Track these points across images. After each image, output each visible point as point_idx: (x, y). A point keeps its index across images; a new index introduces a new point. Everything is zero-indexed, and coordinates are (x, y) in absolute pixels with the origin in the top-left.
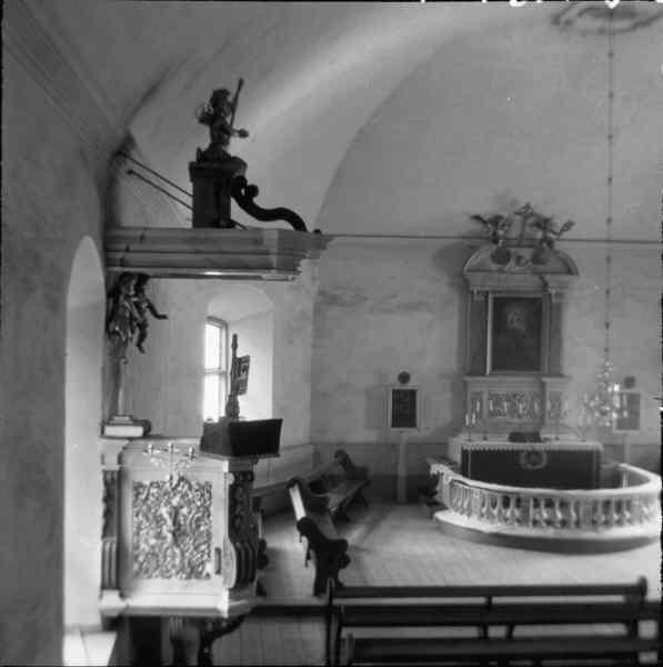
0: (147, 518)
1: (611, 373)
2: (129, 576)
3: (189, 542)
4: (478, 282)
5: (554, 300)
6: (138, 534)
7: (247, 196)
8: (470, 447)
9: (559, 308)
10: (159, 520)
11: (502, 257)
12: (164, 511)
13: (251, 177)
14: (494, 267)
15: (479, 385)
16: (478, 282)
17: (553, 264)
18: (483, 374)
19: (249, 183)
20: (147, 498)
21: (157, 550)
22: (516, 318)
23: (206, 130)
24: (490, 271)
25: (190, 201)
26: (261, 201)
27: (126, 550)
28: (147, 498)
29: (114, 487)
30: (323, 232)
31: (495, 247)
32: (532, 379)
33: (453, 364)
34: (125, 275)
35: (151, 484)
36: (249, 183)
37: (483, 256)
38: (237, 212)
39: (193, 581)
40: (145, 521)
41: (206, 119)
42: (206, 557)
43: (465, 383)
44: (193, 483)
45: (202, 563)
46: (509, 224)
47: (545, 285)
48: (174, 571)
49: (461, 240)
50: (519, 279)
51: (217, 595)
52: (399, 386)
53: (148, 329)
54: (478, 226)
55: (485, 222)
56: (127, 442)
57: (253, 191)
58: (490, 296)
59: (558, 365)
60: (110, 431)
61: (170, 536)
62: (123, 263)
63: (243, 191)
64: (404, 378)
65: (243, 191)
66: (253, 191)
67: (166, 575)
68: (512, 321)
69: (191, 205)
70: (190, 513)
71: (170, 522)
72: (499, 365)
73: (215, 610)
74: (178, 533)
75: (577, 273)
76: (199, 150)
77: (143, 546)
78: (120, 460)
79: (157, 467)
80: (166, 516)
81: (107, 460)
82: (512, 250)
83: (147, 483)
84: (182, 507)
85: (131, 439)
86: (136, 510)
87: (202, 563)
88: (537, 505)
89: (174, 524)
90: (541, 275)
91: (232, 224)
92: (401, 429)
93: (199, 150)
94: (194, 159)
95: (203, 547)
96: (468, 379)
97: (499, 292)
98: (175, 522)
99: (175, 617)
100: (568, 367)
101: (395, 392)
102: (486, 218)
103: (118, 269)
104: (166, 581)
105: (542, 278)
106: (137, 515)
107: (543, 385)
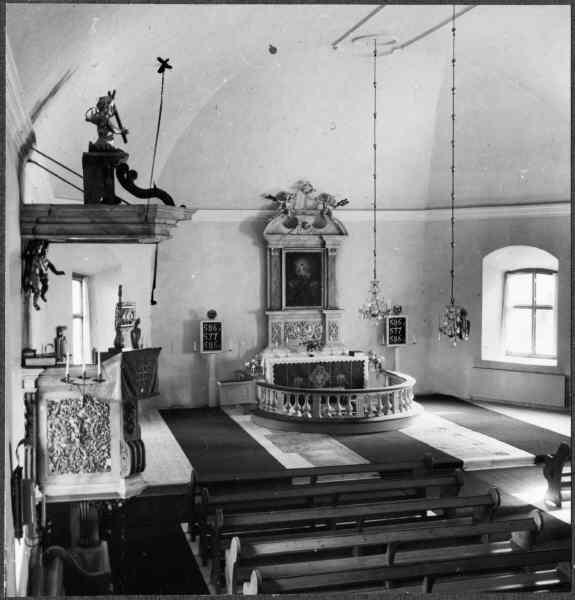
0: (59, 428)
2: (46, 475)
3: (92, 445)
4: (275, 242)
5: (330, 254)
6: (52, 440)
7: (128, 178)
8: (279, 361)
9: (334, 259)
10: (70, 429)
11: (292, 224)
12: (72, 421)
13: (132, 164)
14: (286, 230)
15: (278, 318)
16: (275, 242)
17: (330, 228)
18: (280, 309)
19: (130, 169)
20: (59, 413)
21: (67, 452)
22: (302, 267)
23: (94, 128)
24: (283, 234)
25: (80, 183)
26: (142, 183)
27: (43, 451)
28: (59, 413)
29: (32, 403)
30: (188, 206)
31: (285, 217)
32: (316, 312)
33: (256, 304)
34: (37, 240)
35: (62, 402)
36: (130, 169)
37: (277, 223)
38: (120, 191)
39: (97, 473)
40: (57, 430)
41: (93, 120)
42: (106, 455)
43: (267, 317)
44: (94, 399)
45: (104, 459)
46: (293, 197)
47: (323, 244)
48: (81, 467)
49: (422, 216)
51: (115, 482)
53: (49, 283)
54: (270, 202)
55: (274, 199)
56: (41, 371)
57: (134, 174)
58: (284, 252)
60: (29, 362)
61: (78, 440)
62: (34, 232)
63: (125, 175)
65: (125, 175)
66: (134, 174)
67: (75, 471)
69: (82, 187)
70: (92, 421)
71: (77, 431)
73: (116, 494)
74: (84, 437)
75: (346, 234)
76: (91, 143)
77: (56, 448)
78: (36, 386)
79: (57, 393)
80: (74, 425)
81: (26, 385)
82: (298, 217)
83: (57, 400)
84: (86, 418)
85: (45, 367)
86: (50, 422)
87: (104, 459)
88: (324, 401)
89: (81, 431)
90: (321, 236)
91: (118, 201)
93: (91, 143)
94: (86, 150)
95: (104, 447)
96: (267, 313)
98: (82, 430)
99: (83, 502)
100: (341, 302)
102: (274, 195)
103: (30, 237)
104: (76, 475)
105: (321, 238)
106: (51, 427)
107: (324, 316)
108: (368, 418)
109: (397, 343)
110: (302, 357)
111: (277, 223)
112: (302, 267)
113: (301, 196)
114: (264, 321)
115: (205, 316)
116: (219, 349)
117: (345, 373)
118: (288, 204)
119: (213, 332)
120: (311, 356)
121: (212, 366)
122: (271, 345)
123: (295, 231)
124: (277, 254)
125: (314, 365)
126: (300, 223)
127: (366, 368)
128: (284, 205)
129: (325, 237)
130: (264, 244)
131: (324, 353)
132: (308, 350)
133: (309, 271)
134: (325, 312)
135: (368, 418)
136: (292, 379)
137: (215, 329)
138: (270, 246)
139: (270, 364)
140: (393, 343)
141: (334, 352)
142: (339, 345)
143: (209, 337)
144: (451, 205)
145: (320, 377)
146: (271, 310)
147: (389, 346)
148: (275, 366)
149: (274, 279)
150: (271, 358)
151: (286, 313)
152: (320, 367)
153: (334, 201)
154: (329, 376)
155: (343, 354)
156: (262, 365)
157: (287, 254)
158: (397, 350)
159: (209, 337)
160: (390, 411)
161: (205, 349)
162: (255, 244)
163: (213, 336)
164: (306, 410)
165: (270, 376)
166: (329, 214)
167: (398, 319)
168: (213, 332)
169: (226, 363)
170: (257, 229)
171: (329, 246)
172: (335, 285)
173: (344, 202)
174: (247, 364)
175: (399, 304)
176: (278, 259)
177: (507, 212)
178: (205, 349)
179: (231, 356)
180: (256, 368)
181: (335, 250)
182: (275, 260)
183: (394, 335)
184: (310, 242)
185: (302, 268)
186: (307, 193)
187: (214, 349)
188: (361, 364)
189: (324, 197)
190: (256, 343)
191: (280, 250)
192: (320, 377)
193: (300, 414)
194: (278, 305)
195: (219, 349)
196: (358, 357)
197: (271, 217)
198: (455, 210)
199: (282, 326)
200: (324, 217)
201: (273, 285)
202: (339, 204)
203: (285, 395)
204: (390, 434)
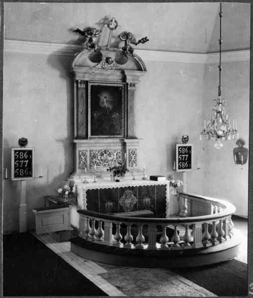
11: (97, 58)
15: (83, 146)
18: (86, 137)
22: (105, 100)
31: (93, 50)
32: (117, 140)
33: (64, 133)
37: (84, 57)
47: (124, 79)
58: (90, 85)
75: (145, 70)
90: (123, 72)
96: (75, 141)
107: (124, 144)
108: (206, 248)
109: (185, 168)
110: (107, 182)
111: (84, 57)
112: (105, 100)
113: (106, 31)
114: (72, 148)
115: (17, 143)
116: (30, 176)
117: (150, 197)
118: (94, 39)
119: (24, 159)
120: (118, 181)
121: (23, 193)
122: (78, 171)
123: (99, 66)
124: (83, 86)
125: (123, 190)
126: (104, 58)
127: (168, 191)
128: (91, 40)
129: (126, 73)
130: (70, 75)
131: (125, 178)
132: (115, 176)
133: (111, 103)
134: (126, 141)
135: (206, 248)
136: (103, 202)
137: (26, 156)
138: (77, 78)
139: (84, 190)
140: (182, 168)
141: (136, 178)
142: (138, 171)
143: (20, 164)
144: (222, 53)
145: (129, 201)
146: (78, 138)
147: (178, 171)
148: (211, 214)
149: (80, 110)
150: (84, 183)
151: (92, 141)
152: (128, 191)
153: (135, 39)
154: (136, 200)
155: (144, 179)
156: (74, 191)
157: (92, 86)
158: (185, 174)
159: (20, 164)
160: (217, 242)
161: (16, 176)
162: (61, 76)
163: (24, 164)
164: (129, 241)
165: (82, 201)
166: (131, 51)
167: (185, 147)
168: (24, 159)
169: (35, 189)
170: (65, 63)
171: (129, 81)
172: (133, 117)
173: (144, 40)
174: (60, 190)
175: (185, 134)
176: (84, 91)
177: (89, 97)
178: (16, 176)
179: (42, 182)
180: (69, 194)
181: (134, 85)
182: (82, 92)
183: (182, 161)
184: (109, 76)
185: (105, 100)
186: (112, 29)
187: (25, 176)
188: (163, 187)
189: (126, 35)
190: (63, 171)
191: (86, 83)
192: (129, 201)
193: (122, 246)
194: (84, 134)
195: (30, 176)
196: (162, 181)
197: (79, 51)
198: (222, 54)
199: (88, 154)
200: (126, 53)
201: (123, 108)
202: (140, 41)
203: (114, 225)
204: (225, 268)
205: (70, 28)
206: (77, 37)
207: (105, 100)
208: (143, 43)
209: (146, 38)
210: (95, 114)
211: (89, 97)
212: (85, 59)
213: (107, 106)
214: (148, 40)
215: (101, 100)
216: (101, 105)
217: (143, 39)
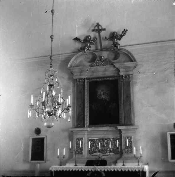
1: (35, 101)
32: (113, 128)
50: (104, 71)
52: (36, 136)
58: (87, 81)
59: (132, 122)
64: (38, 131)
68: (100, 95)
72: (93, 123)
92: (36, 162)
97: (92, 79)
101: (33, 140)
177: (87, 108)
185: (102, 93)
205: (74, 38)
206: (78, 45)
207: (102, 93)
208: (124, 35)
209: (125, 30)
210: (93, 106)
211: (87, 108)
212: (89, 127)
213: (104, 97)
214: (127, 30)
215: (99, 93)
216: (99, 98)
217: (123, 32)
